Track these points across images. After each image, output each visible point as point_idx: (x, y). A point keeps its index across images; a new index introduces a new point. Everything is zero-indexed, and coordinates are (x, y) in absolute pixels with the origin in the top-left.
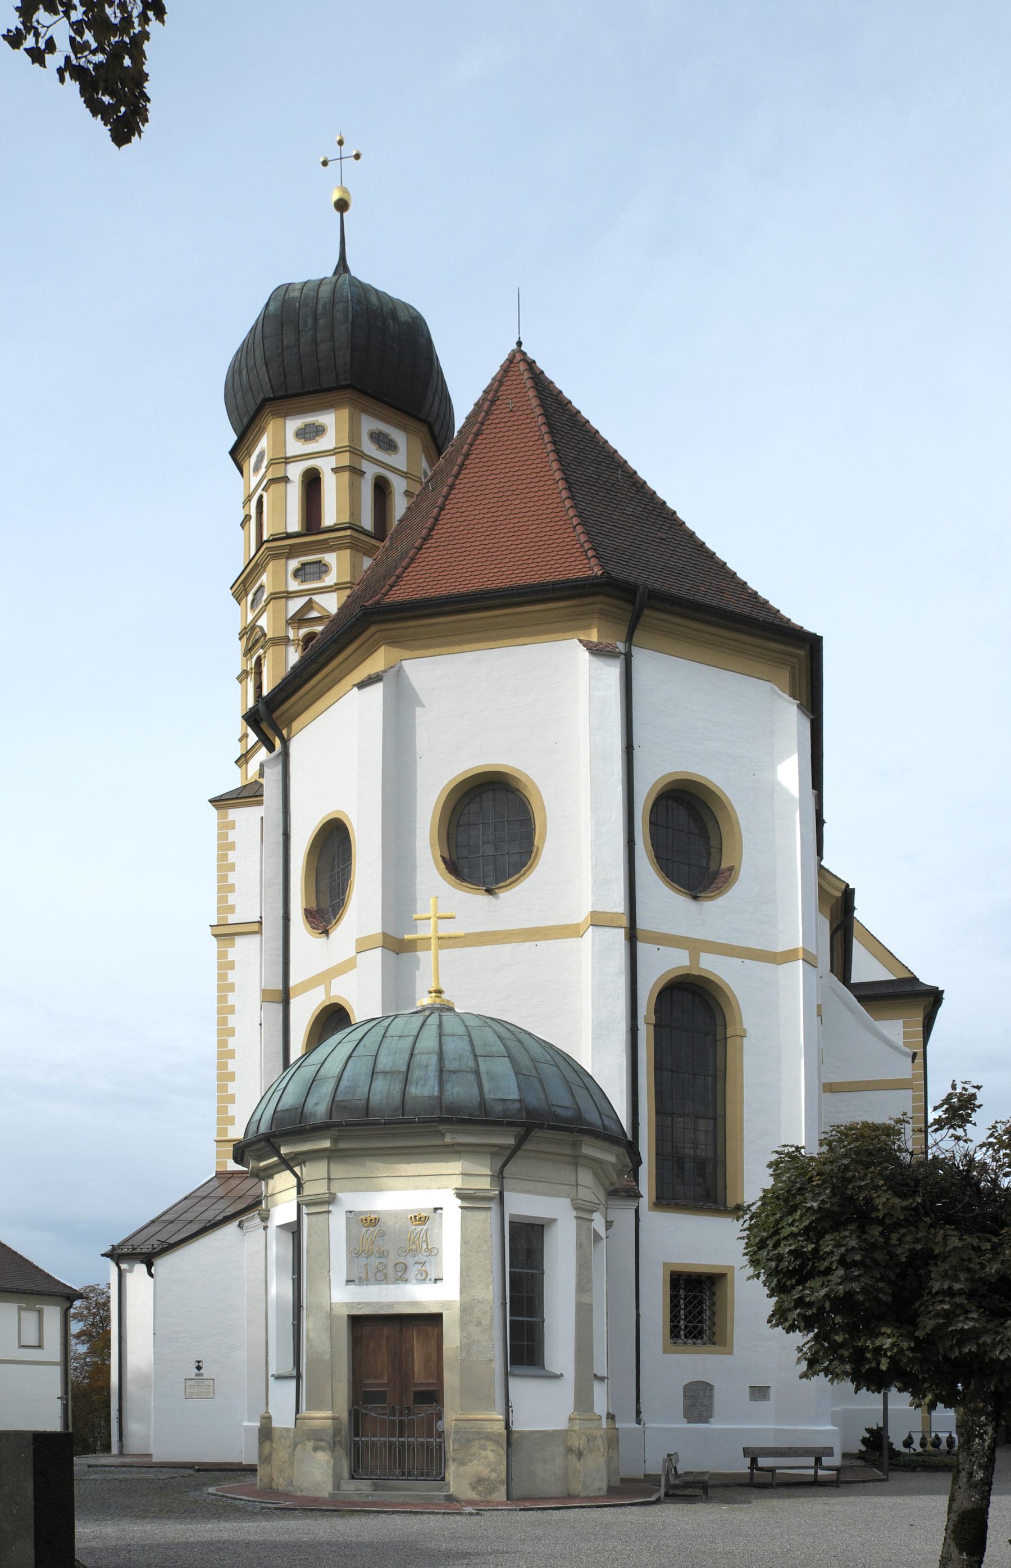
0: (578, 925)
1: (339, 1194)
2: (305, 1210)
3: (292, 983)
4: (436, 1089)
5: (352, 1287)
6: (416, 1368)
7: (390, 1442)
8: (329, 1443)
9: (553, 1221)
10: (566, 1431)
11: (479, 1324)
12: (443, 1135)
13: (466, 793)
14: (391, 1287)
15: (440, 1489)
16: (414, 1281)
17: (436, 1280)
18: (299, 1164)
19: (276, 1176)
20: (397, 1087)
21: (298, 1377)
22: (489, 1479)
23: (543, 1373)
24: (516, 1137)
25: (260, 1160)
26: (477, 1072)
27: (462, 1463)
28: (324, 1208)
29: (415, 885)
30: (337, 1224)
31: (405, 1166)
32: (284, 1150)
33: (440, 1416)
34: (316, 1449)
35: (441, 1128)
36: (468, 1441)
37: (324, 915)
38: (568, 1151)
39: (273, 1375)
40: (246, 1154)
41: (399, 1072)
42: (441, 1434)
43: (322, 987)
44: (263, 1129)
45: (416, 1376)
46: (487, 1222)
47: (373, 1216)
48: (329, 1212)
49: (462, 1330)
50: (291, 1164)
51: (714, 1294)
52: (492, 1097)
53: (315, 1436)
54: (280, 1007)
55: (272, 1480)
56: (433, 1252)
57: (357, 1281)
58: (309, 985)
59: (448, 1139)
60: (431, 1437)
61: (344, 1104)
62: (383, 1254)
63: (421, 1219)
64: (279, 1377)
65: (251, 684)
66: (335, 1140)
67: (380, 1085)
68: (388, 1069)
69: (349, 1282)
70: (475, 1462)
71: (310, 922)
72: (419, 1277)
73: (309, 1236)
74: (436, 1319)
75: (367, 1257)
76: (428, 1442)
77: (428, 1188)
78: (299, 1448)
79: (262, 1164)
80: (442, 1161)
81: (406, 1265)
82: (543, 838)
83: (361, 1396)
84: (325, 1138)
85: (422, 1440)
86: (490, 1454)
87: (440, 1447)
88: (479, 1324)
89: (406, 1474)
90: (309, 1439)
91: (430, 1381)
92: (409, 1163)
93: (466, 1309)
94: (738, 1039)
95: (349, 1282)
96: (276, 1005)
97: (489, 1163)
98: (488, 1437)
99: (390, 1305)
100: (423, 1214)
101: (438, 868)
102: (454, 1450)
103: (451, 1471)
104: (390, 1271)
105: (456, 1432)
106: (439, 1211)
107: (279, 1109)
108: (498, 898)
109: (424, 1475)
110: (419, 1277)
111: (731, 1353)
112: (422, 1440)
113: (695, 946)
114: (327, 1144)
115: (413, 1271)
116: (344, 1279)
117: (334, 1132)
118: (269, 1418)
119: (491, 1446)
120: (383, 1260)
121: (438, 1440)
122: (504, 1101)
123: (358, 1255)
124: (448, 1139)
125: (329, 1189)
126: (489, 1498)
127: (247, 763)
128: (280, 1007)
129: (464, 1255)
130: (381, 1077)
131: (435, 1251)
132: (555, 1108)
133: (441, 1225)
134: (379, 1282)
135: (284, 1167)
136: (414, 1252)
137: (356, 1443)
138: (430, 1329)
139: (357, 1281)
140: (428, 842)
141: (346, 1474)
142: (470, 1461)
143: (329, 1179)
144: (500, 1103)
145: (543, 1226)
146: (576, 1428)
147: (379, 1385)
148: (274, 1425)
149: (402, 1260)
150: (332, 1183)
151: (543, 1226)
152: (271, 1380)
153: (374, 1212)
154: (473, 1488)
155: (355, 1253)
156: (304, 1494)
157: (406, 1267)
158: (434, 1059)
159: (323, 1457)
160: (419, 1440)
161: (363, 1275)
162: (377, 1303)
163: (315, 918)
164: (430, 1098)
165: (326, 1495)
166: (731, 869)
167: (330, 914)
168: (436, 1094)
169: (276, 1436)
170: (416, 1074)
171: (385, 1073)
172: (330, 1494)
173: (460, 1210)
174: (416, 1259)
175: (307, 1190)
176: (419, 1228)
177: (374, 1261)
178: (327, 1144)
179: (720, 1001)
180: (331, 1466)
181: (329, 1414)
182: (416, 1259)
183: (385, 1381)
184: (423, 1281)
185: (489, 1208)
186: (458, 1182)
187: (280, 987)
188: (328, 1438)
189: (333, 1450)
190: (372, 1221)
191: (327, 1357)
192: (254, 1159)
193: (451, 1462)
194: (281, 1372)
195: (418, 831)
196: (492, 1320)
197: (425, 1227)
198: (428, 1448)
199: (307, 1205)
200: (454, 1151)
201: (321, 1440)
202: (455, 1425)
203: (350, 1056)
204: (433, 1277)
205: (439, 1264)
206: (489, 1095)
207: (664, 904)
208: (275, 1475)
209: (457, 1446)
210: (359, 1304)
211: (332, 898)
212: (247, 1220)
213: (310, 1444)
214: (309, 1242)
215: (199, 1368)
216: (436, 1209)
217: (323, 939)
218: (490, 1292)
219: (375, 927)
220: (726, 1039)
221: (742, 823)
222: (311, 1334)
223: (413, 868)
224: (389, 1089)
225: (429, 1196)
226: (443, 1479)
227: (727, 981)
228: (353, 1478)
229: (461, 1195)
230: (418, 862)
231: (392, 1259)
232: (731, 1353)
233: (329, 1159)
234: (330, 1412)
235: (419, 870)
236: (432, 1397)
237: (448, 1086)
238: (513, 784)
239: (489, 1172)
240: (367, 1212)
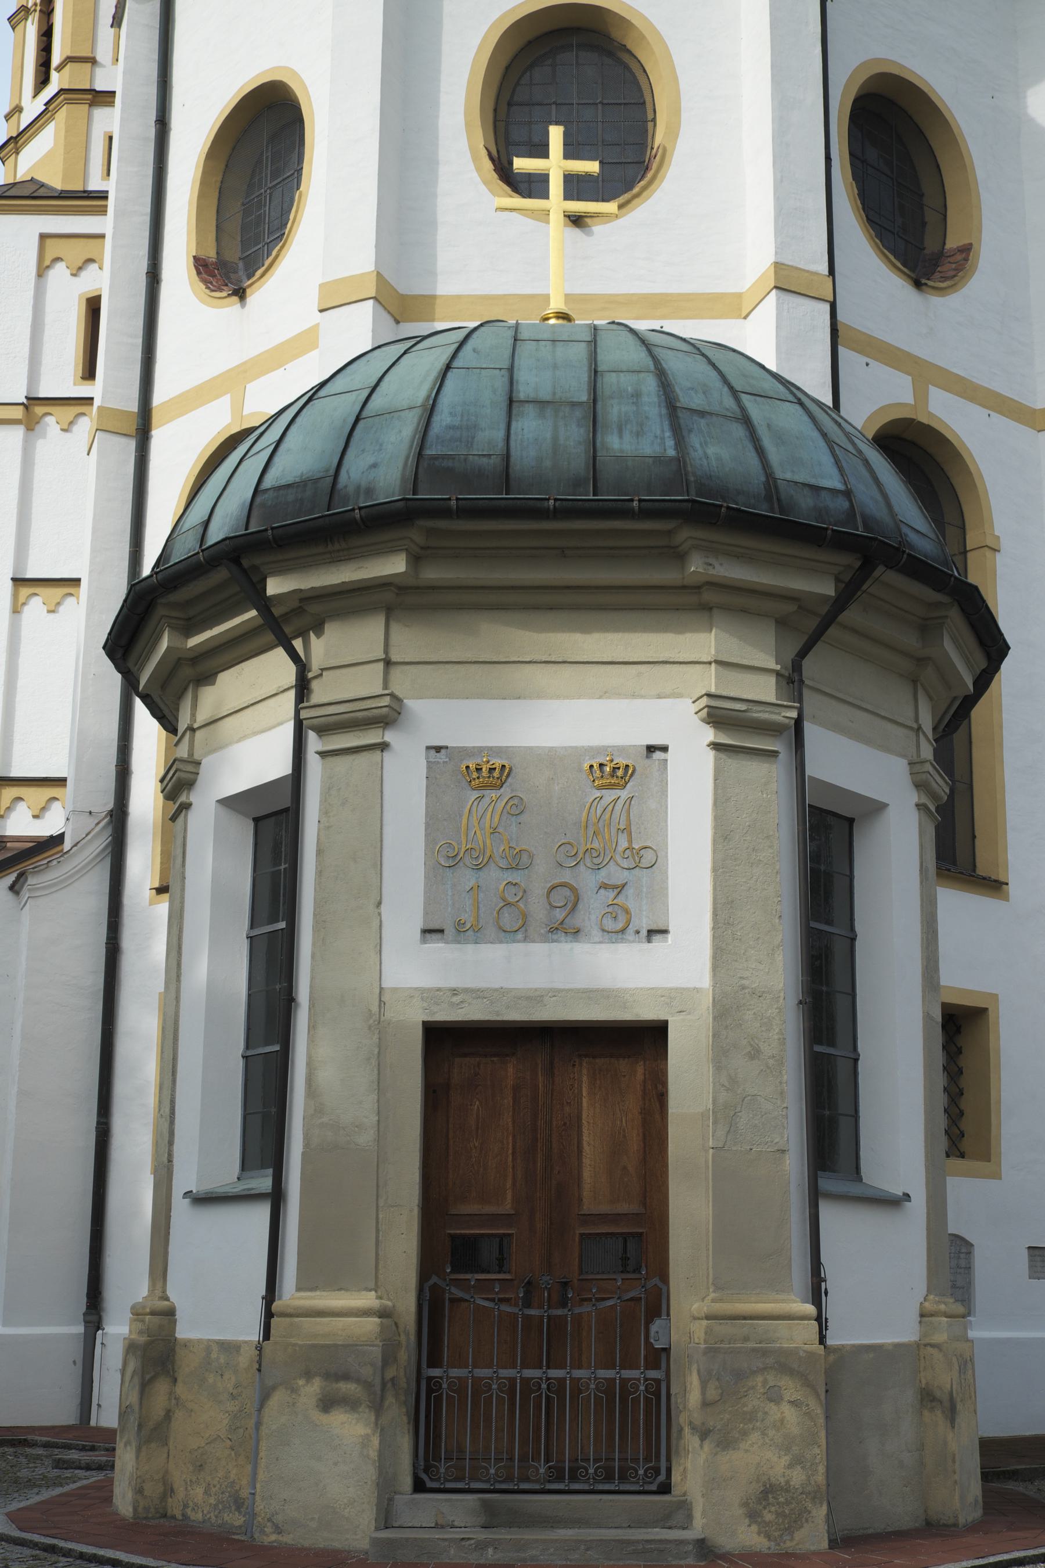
0: (739, 296)
1: (412, 704)
2: (314, 743)
3: (159, 397)
4: (670, 443)
5: (436, 947)
6: (587, 1174)
7: (526, 1381)
8: (367, 1385)
9: (879, 807)
10: (918, 1345)
11: (755, 1054)
12: (680, 557)
13: (530, 42)
14: (539, 949)
15: (665, 1520)
16: (596, 933)
17: (651, 933)
18: (303, 634)
19: (224, 678)
20: (573, 434)
21: (277, 1198)
22: (787, 1488)
23: (854, 1189)
24: (838, 580)
25: (189, 628)
26: (746, 421)
27: (726, 1443)
28: (371, 737)
29: (435, 195)
30: (404, 774)
31: (578, 637)
32: (275, 587)
33: (656, 1305)
34: (327, 1404)
35: (686, 535)
36: (740, 1376)
37: (236, 260)
38: (910, 641)
39: (187, 1194)
40: (160, 611)
41: (574, 405)
42: (659, 1357)
43: (226, 399)
44: (215, 535)
45: (586, 1193)
46: (768, 785)
47: (498, 762)
48: (383, 746)
49: (718, 1067)
50: (288, 630)
51: (960, 1051)
52: (788, 476)
53: (333, 1372)
54: (132, 445)
55: (169, 1491)
56: (646, 859)
57: (450, 931)
58: (194, 399)
59: (696, 566)
60: (629, 1363)
61: (446, 463)
62: (518, 861)
63: (614, 773)
64: (203, 1200)
65: (32, 28)
66: (416, 560)
67: (530, 428)
68: (545, 395)
69: (428, 932)
70: (755, 1437)
71: (205, 281)
72: (609, 924)
73: (325, 811)
74: (648, 1038)
75: (478, 868)
76: (624, 1381)
77: (634, 696)
78: (277, 1399)
79: (194, 641)
80: (665, 629)
81: (574, 890)
82: (674, 132)
83: (450, 1251)
84: (393, 551)
85: (609, 1374)
86: (790, 1414)
87: (657, 1394)
88: (755, 1054)
89: (565, 1476)
90: (308, 1375)
91: (624, 1208)
92: (585, 630)
93: (725, 1011)
94: (988, 553)
95: (428, 932)
96: (123, 440)
97: (772, 641)
98: (785, 1363)
99: (536, 997)
100: (622, 761)
101: (478, 169)
102: (705, 1404)
103: (693, 1467)
104: (537, 907)
105: (711, 1351)
106: (658, 755)
107: (269, 482)
108: (590, 234)
109: (615, 1477)
110: (609, 924)
111: (997, 1175)
112: (609, 1374)
113: (923, 373)
114: (395, 565)
115: (594, 906)
116: (418, 924)
117: (415, 535)
118: (170, 1313)
119: (790, 1388)
120: (515, 877)
121: (653, 1374)
122: (816, 489)
123: (454, 862)
124: (696, 566)
125: (386, 686)
126: (789, 1545)
127: (18, 153)
128: (131, 446)
129: (721, 870)
130: (530, 410)
131: (648, 857)
132: (905, 530)
133: (664, 792)
134: (507, 934)
135: (270, 637)
136: (596, 858)
137: (433, 1386)
138: (623, 1065)
139: (450, 931)
140: (460, 118)
141: (407, 1482)
142: (745, 1434)
143: (388, 663)
144: (806, 491)
145: (851, 821)
146: (940, 1338)
147: (494, 1219)
148: (184, 1331)
149: (566, 877)
150: (396, 673)
151: (851, 821)
152: (180, 1206)
153: (498, 751)
154: (753, 1516)
155: (447, 858)
156: (287, 1539)
157: (574, 903)
158: (650, 384)
159: (352, 1431)
160: (505, 1373)
161: (468, 918)
162: (502, 991)
163: (214, 276)
164: (658, 460)
165: (364, 1544)
166: (966, 250)
167: (241, 273)
168: (671, 452)
169: (187, 1364)
170: (614, 410)
171: (541, 404)
172: (375, 1542)
173: (711, 754)
174: (602, 876)
175: (320, 693)
176: (609, 795)
177: (495, 878)
178: (395, 565)
179: (956, 481)
180: (373, 1454)
181: (367, 1300)
182: (602, 876)
183: (507, 1207)
184: (619, 934)
185: (774, 754)
186: (709, 680)
187: (134, 407)
188: (367, 1372)
189: (378, 1408)
190: (491, 773)
191: (366, 1139)
192: (172, 627)
193: (691, 1440)
194: (210, 1185)
195: (444, 98)
196: (782, 1042)
197: (624, 794)
198: (624, 1400)
199: (322, 731)
200: (696, 603)
201: (346, 1377)
202: (708, 1331)
203: (448, 367)
204: (645, 926)
205: (659, 894)
206: (783, 474)
207: (875, 283)
208: (179, 1477)
209: (712, 1393)
210: (455, 992)
211: (245, 244)
212: (37, 871)
213: (312, 1390)
214: (324, 829)
215: (651, 933)
216: (651, 749)
217: (231, 309)
218: (775, 972)
219: (361, 260)
220: (965, 552)
221: (980, 173)
222: (326, 1076)
223: (432, 164)
224: (555, 439)
225: (634, 714)
226: (665, 1489)
227: (969, 445)
228: (419, 1487)
229: (716, 718)
230: (442, 154)
231: (539, 878)
232: (997, 1175)
233: (390, 612)
234: (365, 1302)
235: (443, 170)
236: (638, 1246)
237: (694, 440)
238: (616, 34)
239: (772, 665)
240: (481, 750)
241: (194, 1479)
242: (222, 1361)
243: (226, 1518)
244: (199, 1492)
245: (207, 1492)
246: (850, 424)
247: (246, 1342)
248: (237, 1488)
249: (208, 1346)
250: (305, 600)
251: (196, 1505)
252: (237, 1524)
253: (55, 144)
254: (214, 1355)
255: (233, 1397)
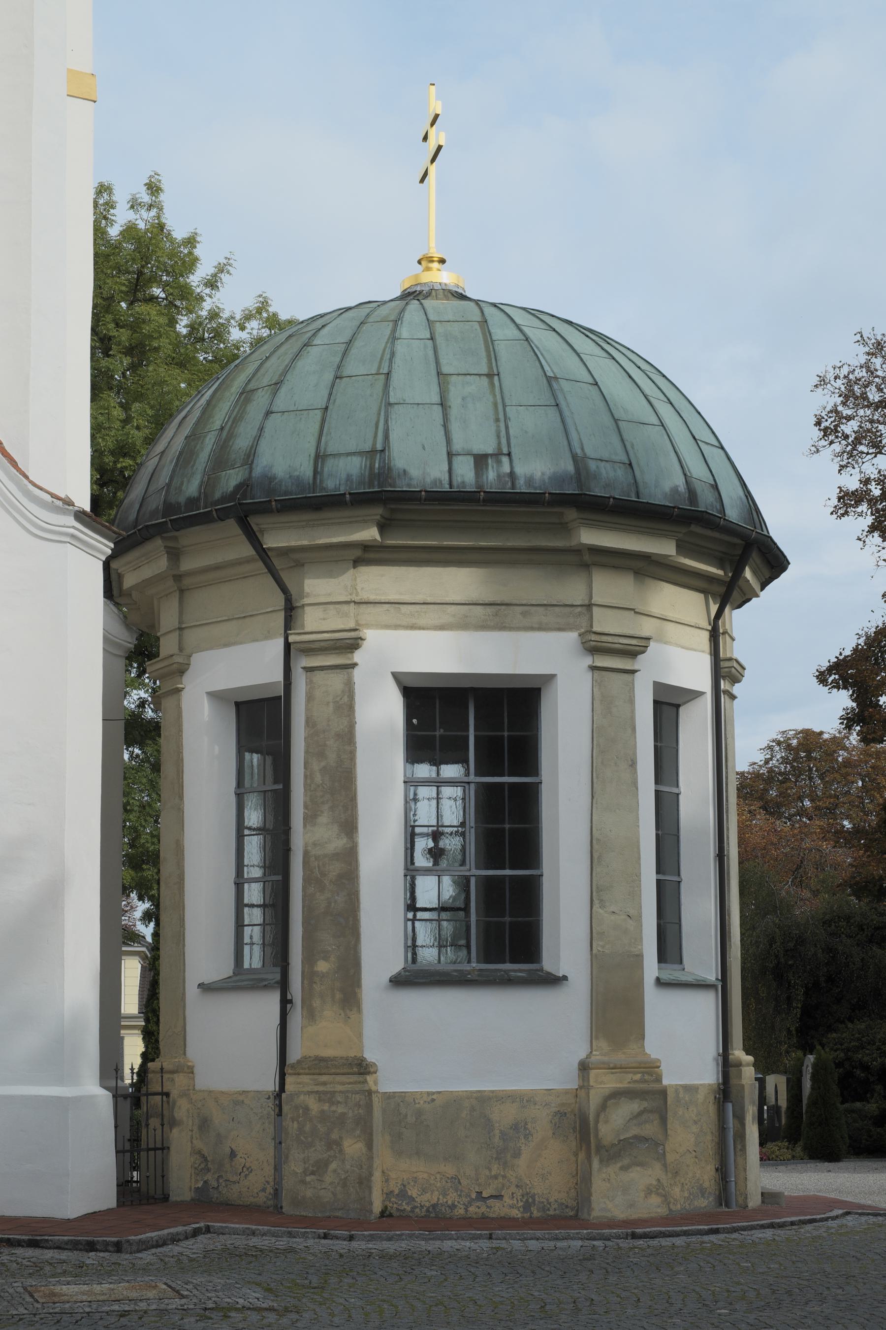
178: (371, 534)
241: (144, 263)
242: (687, 1099)
243: (696, 1203)
244: (677, 1191)
245: (682, 1191)
246: (41, 489)
247: (701, 1085)
248: (701, 1182)
249: (677, 1088)
250: (596, 550)
251: (675, 1200)
252: (703, 1205)
253: (146, 1047)
254: (681, 1095)
255: (695, 1122)
